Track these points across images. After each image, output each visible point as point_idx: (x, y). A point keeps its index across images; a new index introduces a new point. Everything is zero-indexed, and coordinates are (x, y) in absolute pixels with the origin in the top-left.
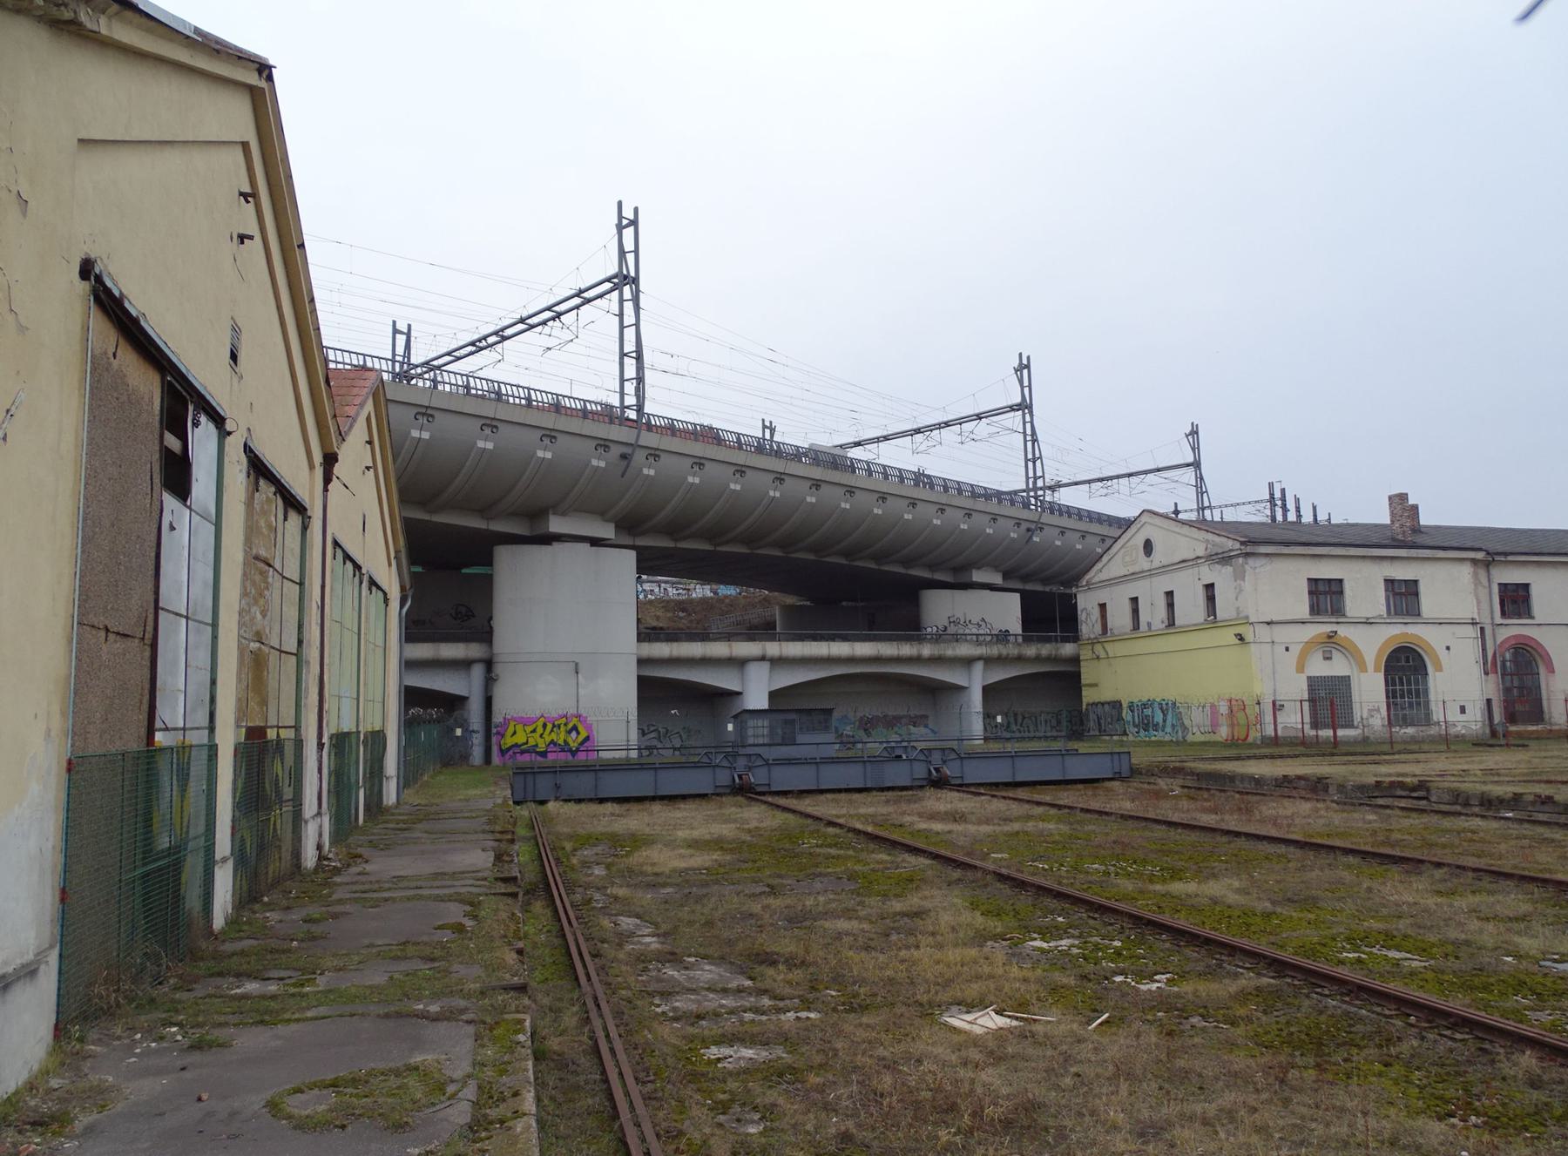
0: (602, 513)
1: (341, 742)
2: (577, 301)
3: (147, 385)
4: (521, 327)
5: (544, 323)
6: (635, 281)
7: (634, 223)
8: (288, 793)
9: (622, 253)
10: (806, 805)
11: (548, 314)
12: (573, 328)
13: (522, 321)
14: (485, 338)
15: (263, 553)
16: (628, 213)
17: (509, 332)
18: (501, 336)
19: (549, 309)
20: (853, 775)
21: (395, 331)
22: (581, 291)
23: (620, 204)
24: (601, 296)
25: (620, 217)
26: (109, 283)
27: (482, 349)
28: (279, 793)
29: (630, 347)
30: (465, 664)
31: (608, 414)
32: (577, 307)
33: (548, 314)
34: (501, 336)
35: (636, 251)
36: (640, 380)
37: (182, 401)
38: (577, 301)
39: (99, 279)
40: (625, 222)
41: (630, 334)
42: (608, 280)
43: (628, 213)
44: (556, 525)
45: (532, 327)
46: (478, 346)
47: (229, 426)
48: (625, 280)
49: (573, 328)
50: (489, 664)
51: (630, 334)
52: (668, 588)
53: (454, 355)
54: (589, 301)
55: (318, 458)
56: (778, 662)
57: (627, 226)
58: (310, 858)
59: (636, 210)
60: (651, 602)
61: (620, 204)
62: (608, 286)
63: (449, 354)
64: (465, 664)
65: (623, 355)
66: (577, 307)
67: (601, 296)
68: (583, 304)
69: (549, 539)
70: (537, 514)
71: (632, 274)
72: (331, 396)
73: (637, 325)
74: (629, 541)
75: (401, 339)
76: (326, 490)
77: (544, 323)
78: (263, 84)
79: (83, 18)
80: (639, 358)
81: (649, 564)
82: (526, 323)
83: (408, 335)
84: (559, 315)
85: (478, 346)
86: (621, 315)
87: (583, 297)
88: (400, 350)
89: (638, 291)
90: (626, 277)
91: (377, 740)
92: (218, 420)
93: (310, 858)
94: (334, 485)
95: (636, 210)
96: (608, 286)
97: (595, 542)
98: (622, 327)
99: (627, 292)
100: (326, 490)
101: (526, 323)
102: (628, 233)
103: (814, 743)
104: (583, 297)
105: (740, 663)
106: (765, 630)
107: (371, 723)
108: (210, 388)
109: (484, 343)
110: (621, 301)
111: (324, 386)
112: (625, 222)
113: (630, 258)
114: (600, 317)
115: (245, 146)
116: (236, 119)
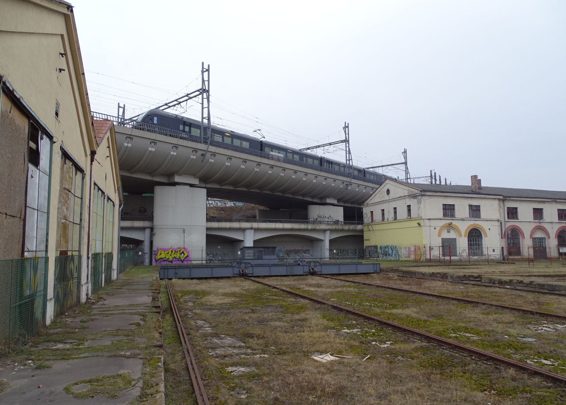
0: (194, 175)
2: (186, 98)
3: (23, 124)
5: (174, 105)
6: (208, 91)
7: (208, 70)
8: (75, 275)
9: (203, 81)
11: (176, 102)
13: (166, 104)
15: (67, 187)
16: (206, 67)
19: (176, 100)
20: (282, 270)
21: (119, 107)
23: (203, 63)
24: (195, 96)
25: (203, 68)
26: (8, 85)
30: (143, 229)
33: (176, 102)
38: (186, 98)
40: (204, 70)
41: (206, 111)
42: (198, 91)
43: (206, 67)
44: (177, 179)
47: (54, 140)
48: (204, 91)
50: (152, 229)
51: (206, 111)
52: (218, 203)
54: (191, 98)
55: (89, 152)
56: (257, 230)
57: (205, 71)
58: (83, 299)
59: (209, 66)
60: (212, 207)
61: (203, 63)
62: (198, 93)
64: (143, 229)
66: (187, 100)
68: (189, 99)
69: (174, 184)
70: (171, 175)
71: (207, 89)
72: (94, 130)
73: (208, 107)
74: (204, 185)
76: (91, 164)
77: (174, 105)
78: (69, 13)
81: (211, 194)
84: (180, 103)
86: (202, 104)
87: (189, 97)
89: (209, 95)
90: (204, 90)
92: (50, 137)
93: (83, 299)
95: (209, 66)
96: (198, 93)
97: (192, 186)
98: (203, 108)
100: (91, 164)
104: (189, 97)
105: (243, 230)
106: (252, 218)
107: (108, 250)
110: (203, 98)
111: (91, 126)
112: (204, 70)
113: (206, 83)
115: (62, 36)
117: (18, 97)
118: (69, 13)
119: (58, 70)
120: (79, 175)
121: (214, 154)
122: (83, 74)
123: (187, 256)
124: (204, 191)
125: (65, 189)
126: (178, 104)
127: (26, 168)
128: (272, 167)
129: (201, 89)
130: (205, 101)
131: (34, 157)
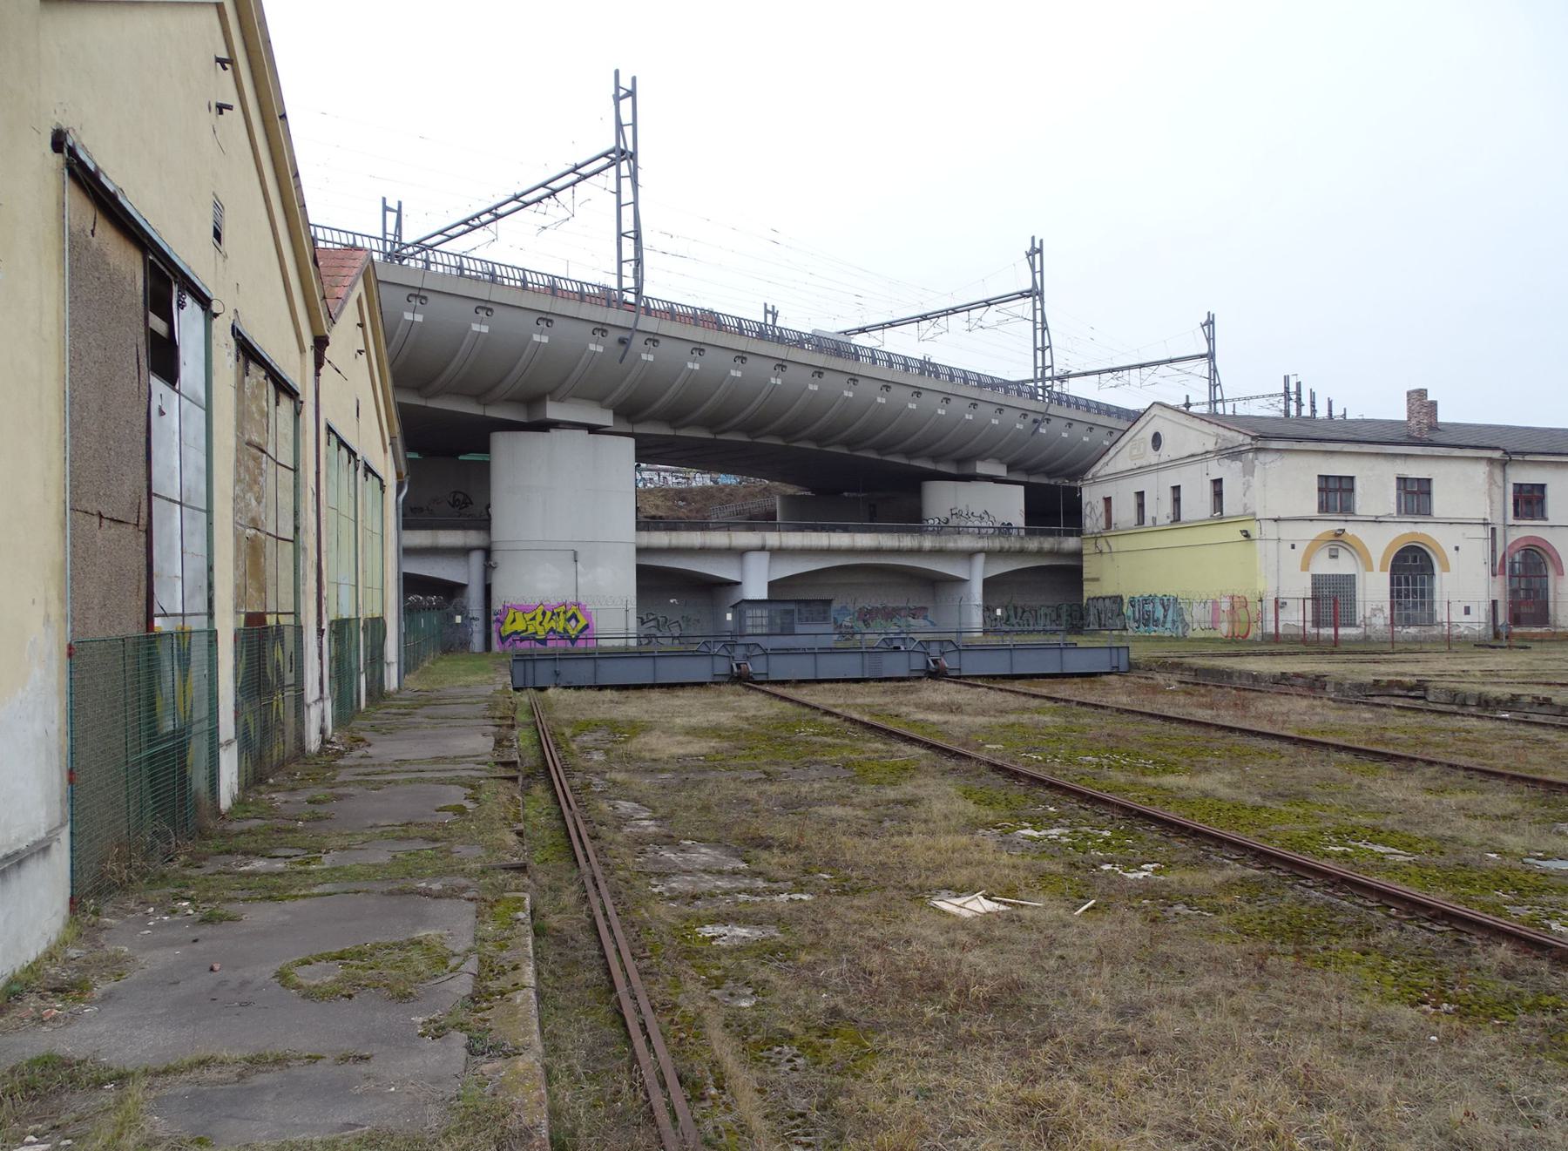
0: (600, 400)
2: (573, 177)
3: (129, 265)
4: (515, 204)
5: (539, 200)
6: (633, 156)
7: (632, 93)
9: (619, 126)
10: (804, 694)
11: (543, 192)
13: (516, 198)
14: (478, 216)
16: (626, 83)
17: (501, 210)
19: (544, 185)
21: (386, 209)
22: (577, 167)
23: (617, 72)
24: (597, 172)
25: (618, 87)
27: (475, 228)
32: (573, 184)
33: (543, 192)
35: (634, 125)
36: (638, 261)
38: (573, 177)
41: (628, 212)
42: (605, 155)
43: (626, 83)
44: (553, 411)
45: (527, 204)
46: (471, 224)
48: (622, 155)
49: (569, 206)
50: (488, 552)
51: (628, 212)
52: (667, 477)
53: (446, 234)
54: (585, 177)
55: (308, 342)
56: (777, 552)
57: (624, 97)
59: (634, 80)
61: (617, 72)
62: (604, 161)
63: (441, 233)
64: (465, 552)
66: (573, 184)
67: (597, 172)
69: (545, 426)
70: (534, 400)
71: (630, 148)
72: (319, 277)
75: (392, 217)
76: (317, 374)
77: (539, 200)
80: (637, 238)
81: (647, 452)
82: (520, 201)
84: (554, 192)
86: (618, 193)
88: (391, 228)
90: (623, 152)
91: (376, 626)
92: (204, 301)
94: (326, 370)
95: (634, 80)
96: (604, 161)
97: (593, 429)
98: (619, 206)
100: (317, 374)
104: (578, 173)
105: (740, 553)
109: (477, 222)
110: (619, 177)
111: (312, 265)
112: (622, 92)
113: (628, 131)
114: (598, 193)
121: (654, 339)
124: (629, 444)
126: (548, 196)
127: (144, 387)
129: (612, 151)
130: (626, 184)
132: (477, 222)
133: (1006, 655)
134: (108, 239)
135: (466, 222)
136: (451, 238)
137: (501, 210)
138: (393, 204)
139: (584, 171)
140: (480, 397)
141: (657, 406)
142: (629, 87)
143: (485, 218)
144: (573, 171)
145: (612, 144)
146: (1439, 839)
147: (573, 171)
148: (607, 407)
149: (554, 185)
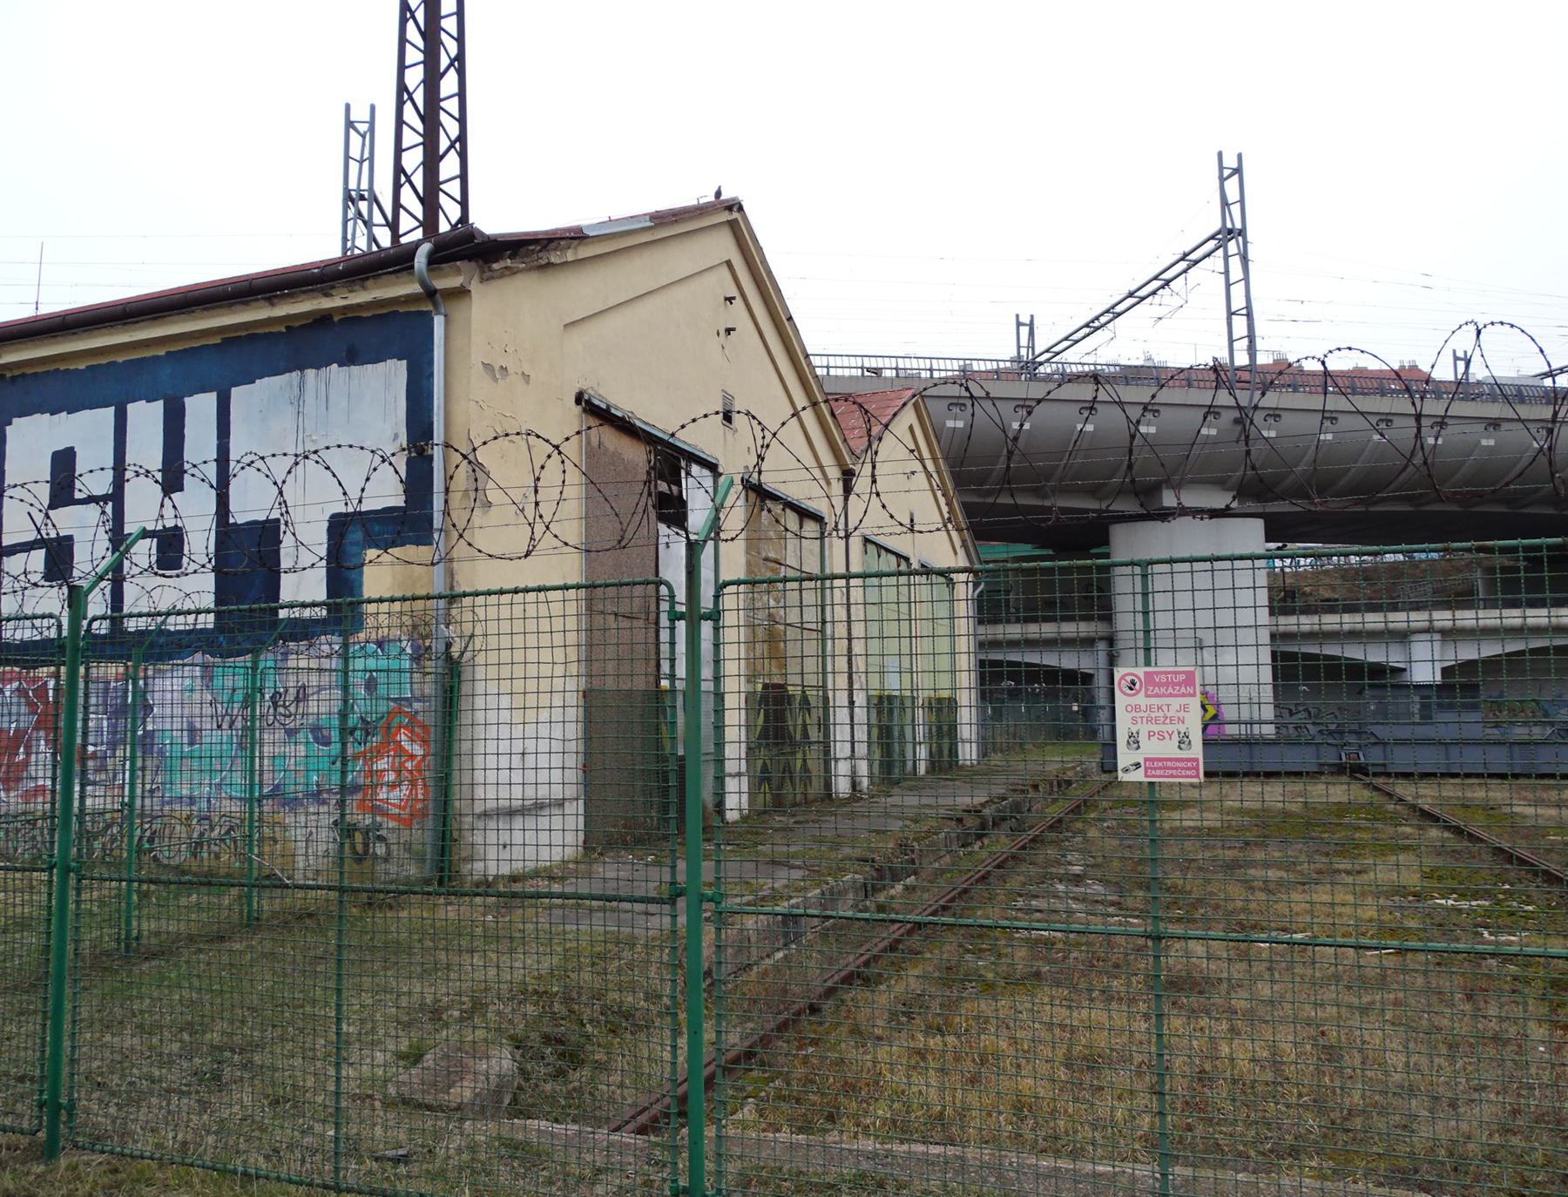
0: (1220, 483)
1: (884, 705)
2: (1183, 265)
3: (636, 455)
4: (1131, 301)
5: (1154, 293)
6: (1242, 232)
7: (1238, 171)
8: (814, 735)
9: (1225, 204)
10: (1403, 789)
11: (1156, 284)
12: (1182, 293)
13: (1131, 295)
14: (1097, 318)
15: (772, 555)
16: (1230, 162)
17: (1118, 309)
18: (1113, 313)
19: (1156, 278)
20: (1498, 759)
21: (1019, 324)
22: (1186, 255)
23: (1220, 155)
24: (1208, 255)
25: (1221, 168)
26: (596, 402)
27: (1097, 329)
28: (805, 734)
29: (1238, 302)
30: (1088, 643)
31: (1219, 374)
32: (1185, 271)
33: (1156, 284)
34: (1113, 313)
35: (1242, 201)
36: (1251, 337)
37: (670, 460)
38: (1183, 265)
39: (589, 402)
40: (1226, 173)
41: (1238, 292)
42: (1213, 237)
43: (1230, 162)
44: (1169, 499)
45: (1143, 299)
46: (1092, 326)
47: (721, 470)
48: (1227, 234)
49: (1182, 293)
50: (1111, 640)
51: (1238, 292)
52: (1301, 560)
53: (1071, 340)
54: (1196, 262)
55: (834, 473)
56: (1451, 635)
57: (1230, 176)
58: (842, 786)
59: (1240, 156)
60: (1327, 571)
61: (1220, 155)
62: (1212, 244)
63: (1066, 339)
64: (1088, 643)
65: (1230, 314)
66: (1185, 271)
67: (1208, 255)
68: (1189, 268)
69: (1165, 515)
70: (1154, 490)
71: (1238, 225)
72: (838, 425)
73: (1246, 278)
74: (1251, 506)
75: (1024, 331)
76: (846, 499)
77: (1154, 293)
78: (736, 215)
79: (553, 260)
80: (1249, 316)
81: (1277, 530)
82: (1136, 297)
83: (1031, 325)
84: (1168, 282)
85: (1092, 326)
86: (1227, 273)
87: (1188, 260)
88: (1024, 341)
89: (1245, 243)
90: (1230, 231)
91: (943, 709)
92: (712, 467)
93: (842, 786)
94: (852, 497)
95: (1240, 156)
96: (1212, 244)
97: (1215, 514)
98: (1228, 285)
99: (1232, 247)
100: (846, 499)
101: (1136, 297)
102: (1232, 186)
103: (1471, 724)
104: (1188, 260)
105: (1403, 637)
106: (1462, 599)
107: (927, 686)
108: (700, 446)
109: (1097, 324)
110: (1226, 257)
111: (847, 411)
112: (1226, 173)
113: (1236, 209)
114: (1208, 276)
115: (729, 263)
116: (722, 246)
117: (619, 414)
118: (736, 215)
119: (722, 332)
120: (811, 528)
121: (1275, 414)
122: (790, 319)
123: (1215, 717)
124: (1258, 525)
125: (766, 559)
126: (1162, 287)
127: (653, 532)
128: (1495, 423)
129: (1219, 233)
130: (1235, 263)
131: (673, 511)
132: (1097, 324)
133: (1246, 749)
134: (611, 439)
135: (1087, 325)
136: (1077, 342)
137: (1118, 309)
138: (1025, 319)
139: (1193, 257)
140: (1094, 492)
141: (1288, 481)
142: (1235, 166)
143: (1103, 319)
144: (1182, 259)
145: (1217, 226)
146: (1195, 921)
147: (1182, 259)
148: (1229, 490)
149: (1167, 276)
